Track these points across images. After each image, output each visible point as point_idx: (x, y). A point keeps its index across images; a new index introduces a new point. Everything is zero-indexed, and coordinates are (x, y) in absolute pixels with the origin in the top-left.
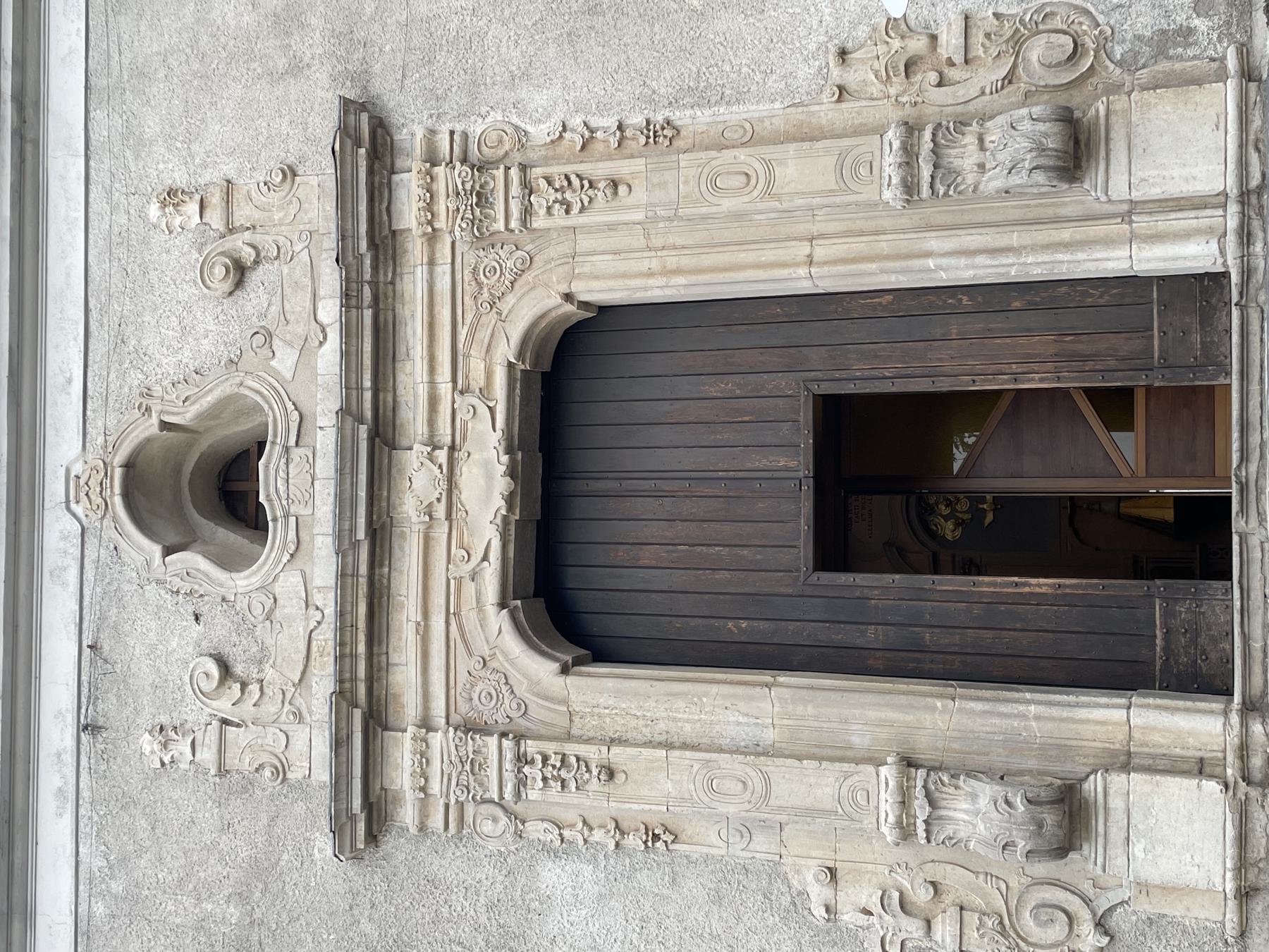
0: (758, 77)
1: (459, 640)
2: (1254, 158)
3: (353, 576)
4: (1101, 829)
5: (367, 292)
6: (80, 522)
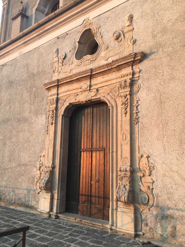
0: (145, 140)
3: (131, 58)
4: (45, 194)
5: (110, 68)
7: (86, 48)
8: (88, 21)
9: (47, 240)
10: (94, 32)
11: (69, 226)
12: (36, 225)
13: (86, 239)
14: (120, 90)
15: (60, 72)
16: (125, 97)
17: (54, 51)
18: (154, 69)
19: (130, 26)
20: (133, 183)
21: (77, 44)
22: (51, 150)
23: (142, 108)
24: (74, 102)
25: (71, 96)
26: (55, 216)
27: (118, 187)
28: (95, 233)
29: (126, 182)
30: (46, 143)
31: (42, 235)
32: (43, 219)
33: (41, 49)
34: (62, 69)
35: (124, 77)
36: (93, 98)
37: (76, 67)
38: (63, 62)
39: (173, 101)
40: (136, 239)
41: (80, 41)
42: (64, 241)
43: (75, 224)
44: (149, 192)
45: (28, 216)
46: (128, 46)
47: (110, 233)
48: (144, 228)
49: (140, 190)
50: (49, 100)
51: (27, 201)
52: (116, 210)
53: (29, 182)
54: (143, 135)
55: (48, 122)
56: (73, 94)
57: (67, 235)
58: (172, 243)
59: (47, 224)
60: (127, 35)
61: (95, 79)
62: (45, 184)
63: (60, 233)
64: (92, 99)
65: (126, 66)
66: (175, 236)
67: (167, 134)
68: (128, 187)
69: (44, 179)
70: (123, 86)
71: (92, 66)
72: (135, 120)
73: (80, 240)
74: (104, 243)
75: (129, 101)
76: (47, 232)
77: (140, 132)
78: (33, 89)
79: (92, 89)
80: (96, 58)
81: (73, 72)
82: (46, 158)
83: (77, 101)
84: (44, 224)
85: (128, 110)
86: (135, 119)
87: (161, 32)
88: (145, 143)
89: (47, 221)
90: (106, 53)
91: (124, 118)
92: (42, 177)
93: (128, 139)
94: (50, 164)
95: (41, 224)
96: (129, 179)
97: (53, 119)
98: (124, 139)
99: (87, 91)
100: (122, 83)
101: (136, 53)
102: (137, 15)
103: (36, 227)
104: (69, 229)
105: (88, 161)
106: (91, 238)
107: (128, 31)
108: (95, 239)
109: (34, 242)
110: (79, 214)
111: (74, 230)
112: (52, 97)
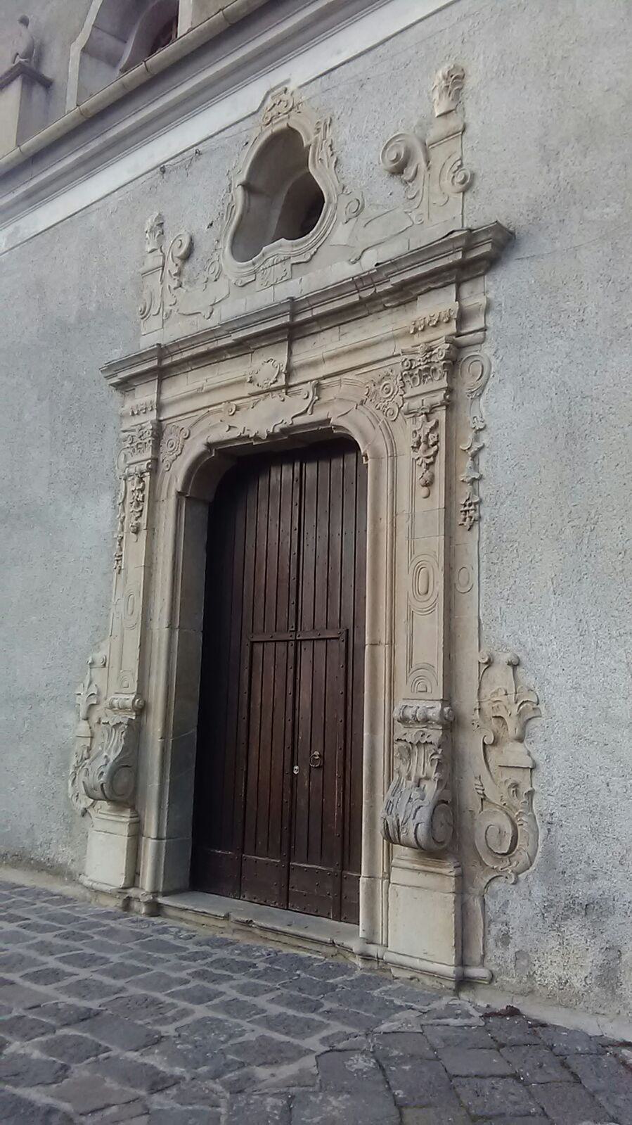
1: (197, 418)
2: (408, 975)
3: (373, 283)
5: (368, 293)
6: (260, 107)
7: (277, 213)
8: (284, 97)
9: (102, 990)
10: (305, 144)
11: (199, 944)
12: (67, 938)
13: (255, 991)
14: (408, 388)
15: (168, 316)
16: (426, 414)
17: (147, 228)
18: (546, 297)
19: (453, 116)
20: (453, 770)
21: (239, 193)
22: (134, 637)
23: (495, 459)
24: (226, 438)
25: (213, 412)
26: (147, 903)
27: (393, 785)
28: (298, 972)
29: (423, 765)
30: (113, 611)
31: (84, 974)
32: (97, 915)
33: (93, 218)
34: (179, 299)
35: (423, 330)
36: (299, 421)
37: (234, 290)
38: (179, 274)
39: (620, 431)
40: (462, 995)
41: (252, 183)
42: (168, 995)
43: (225, 936)
44: (519, 802)
45: (39, 905)
46: (440, 200)
47: (358, 973)
48: (495, 952)
49: (482, 799)
50: (124, 431)
51: (38, 843)
52: (385, 881)
53: (47, 766)
54: (499, 572)
55: (122, 522)
56: (219, 407)
57: (183, 974)
58: (605, 1011)
59: (111, 933)
60: (438, 154)
61: (309, 342)
62: (108, 777)
63: (157, 969)
64: (295, 423)
65: (432, 286)
66: (617, 987)
67: (593, 566)
68: (431, 788)
69: (105, 754)
70: (420, 368)
71: (298, 287)
72: (465, 511)
73: (234, 994)
74: (328, 1005)
75: (442, 431)
76: (107, 961)
77: (484, 558)
78: (63, 385)
79: (295, 385)
80: (315, 253)
81: (220, 311)
82: (114, 671)
83: (235, 434)
84: (100, 933)
85: (440, 469)
86: (467, 508)
87: (578, 140)
88: (504, 607)
89: (112, 924)
90: (353, 230)
91: (422, 504)
92: (96, 748)
93: (437, 588)
94: (128, 699)
95: (88, 932)
96: (436, 753)
97: (141, 511)
98: (422, 589)
99: (275, 394)
100: (417, 358)
101: (470, 230)
102: (481, 67)
103: (66, 942)
104: (197, 952)
105: (280, 683)
106: (279, 989)
107: (445, 135)
108: (295, 993)
109: (48, 998)
110: (246, 898)
111: (214, 958)
112: (137, 420)
